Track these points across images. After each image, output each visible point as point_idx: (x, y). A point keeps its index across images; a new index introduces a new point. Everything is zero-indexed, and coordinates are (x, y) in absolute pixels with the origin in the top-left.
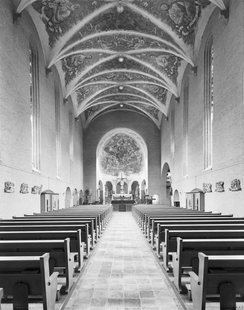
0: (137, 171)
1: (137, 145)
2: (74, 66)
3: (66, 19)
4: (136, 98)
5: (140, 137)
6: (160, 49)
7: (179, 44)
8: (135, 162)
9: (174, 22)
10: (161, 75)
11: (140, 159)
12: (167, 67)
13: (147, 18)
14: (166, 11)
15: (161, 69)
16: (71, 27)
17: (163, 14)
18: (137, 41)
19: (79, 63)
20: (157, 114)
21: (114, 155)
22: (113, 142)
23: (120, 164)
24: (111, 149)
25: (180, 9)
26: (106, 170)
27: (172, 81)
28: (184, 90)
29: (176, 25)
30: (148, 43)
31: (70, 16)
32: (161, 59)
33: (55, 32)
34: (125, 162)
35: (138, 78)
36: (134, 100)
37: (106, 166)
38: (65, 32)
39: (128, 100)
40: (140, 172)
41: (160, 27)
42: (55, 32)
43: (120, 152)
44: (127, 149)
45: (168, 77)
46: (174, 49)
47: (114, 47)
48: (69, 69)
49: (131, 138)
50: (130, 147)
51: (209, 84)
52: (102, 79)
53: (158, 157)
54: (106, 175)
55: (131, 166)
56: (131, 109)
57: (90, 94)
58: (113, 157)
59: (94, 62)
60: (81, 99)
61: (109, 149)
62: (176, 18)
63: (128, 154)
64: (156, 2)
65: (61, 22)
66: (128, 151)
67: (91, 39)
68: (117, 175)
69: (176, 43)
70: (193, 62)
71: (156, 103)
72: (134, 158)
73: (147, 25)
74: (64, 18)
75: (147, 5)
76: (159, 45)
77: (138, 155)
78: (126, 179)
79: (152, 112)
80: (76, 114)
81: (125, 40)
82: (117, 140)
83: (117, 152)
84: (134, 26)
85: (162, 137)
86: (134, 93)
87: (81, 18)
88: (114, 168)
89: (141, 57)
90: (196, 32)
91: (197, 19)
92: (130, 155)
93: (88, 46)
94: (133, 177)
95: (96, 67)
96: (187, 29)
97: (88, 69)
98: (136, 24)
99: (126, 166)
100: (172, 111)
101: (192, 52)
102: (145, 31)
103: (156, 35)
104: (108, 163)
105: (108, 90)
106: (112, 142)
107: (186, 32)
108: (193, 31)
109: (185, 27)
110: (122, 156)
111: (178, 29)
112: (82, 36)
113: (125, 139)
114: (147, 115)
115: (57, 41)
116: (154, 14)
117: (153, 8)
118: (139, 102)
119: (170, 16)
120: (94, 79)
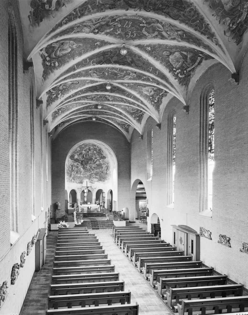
0: (102, 179)
1: (103, 153)
2: (58, 90)
3: (65, 55)
4: (110, 114)
5: (109, 148)
6: (151, 83)
7: (173, 84)
8: (101, 170)
9: (172, 65)
10: (145, 102)
11: (106, 168)
12: (152, 96)
13: (147, 59)
14: (167, 56)
15: (146, 97)
16: (68, 62)
17: (163, 58)
18: (129, 74)
19: (64, 87)
20: (128, 128)
21: (79, 162)
22: (79, 149)
23: (84, 171)
24: (76, 157)
25: (181, 56)
26: (71, 179)
27: (155, 108)
28: (168, 119)
29: (174, 68)
30: (139, 77)
31: (69, 53)
32: (148, 89)
33: (50, 65)
34: (90, 170)
35: (118, 100)
36: (107, 115)
37: (71, 174)
38: (61, 66)
39: (101, 115)
40: (106, 181)
41: (157, 67)
42: (50, 65)
43: (85, 159)
44: (93, 157)
45: (152, 104)
46: (166, 86)
47: (103, 76)
48: (52, 93)
49: (97, 147)
50: (96, 155)
51: (206, 130)
52: (82, 99)
53: (128, 170)
54: (71, 183)
55: (96, 174)
56: (102, 121)
57: (66, 110)
58: (78, 164)
59: (79, 86)
60: (56, 114)
61: (74, 157)
62: (175, 63)
63: (93, 161)
64: (159, 49)
65: (59, 57)
66: (93, 159)
67: (83, 71)
68: (81, 182)
69: (170, 83)
70: (186, 101)
71: (131, 121)
72: (100, 166)
73: (144, 64)
74: (63, 54)
75: (149, 50)
76: (151, 80)
77: (104, 164)
78: (91, 187)
79: (123, 126)
80: (49, 129)
81: (116, 72)
82: (83, 148)
83: (82, 159)
84: (130, 63)
85: (132, 151)
86: (110, 110)
87: (80, 54)
88: (78, 175)
89: (128, 86)
90: (193, 76)
91: (197, 66)
92: (95, 163)
93: (78, 76)
94: (97, 185)
95: (80, 91)
96: (184, 73)
97: (72, 92)
98: (132, 62)
99: (90, 174)
100: (148, 132)
101: (185, 92)
102: (140, 68)
103: (151, 73)
104: (73, 171)
105: (84, 107)
106: (78, 150)
107: (182, 75)
108: (189, 75)
109: (182, 70)
110: (87, 163)
111: (175, 71)
112: (76, 68)
113: (91, 148)
114: (117, 128)
115: (51, 73)
116: (155, 57)
117: (155, 52)
118: (113, 117)
119: (170, 60)
120: (75, 100)
